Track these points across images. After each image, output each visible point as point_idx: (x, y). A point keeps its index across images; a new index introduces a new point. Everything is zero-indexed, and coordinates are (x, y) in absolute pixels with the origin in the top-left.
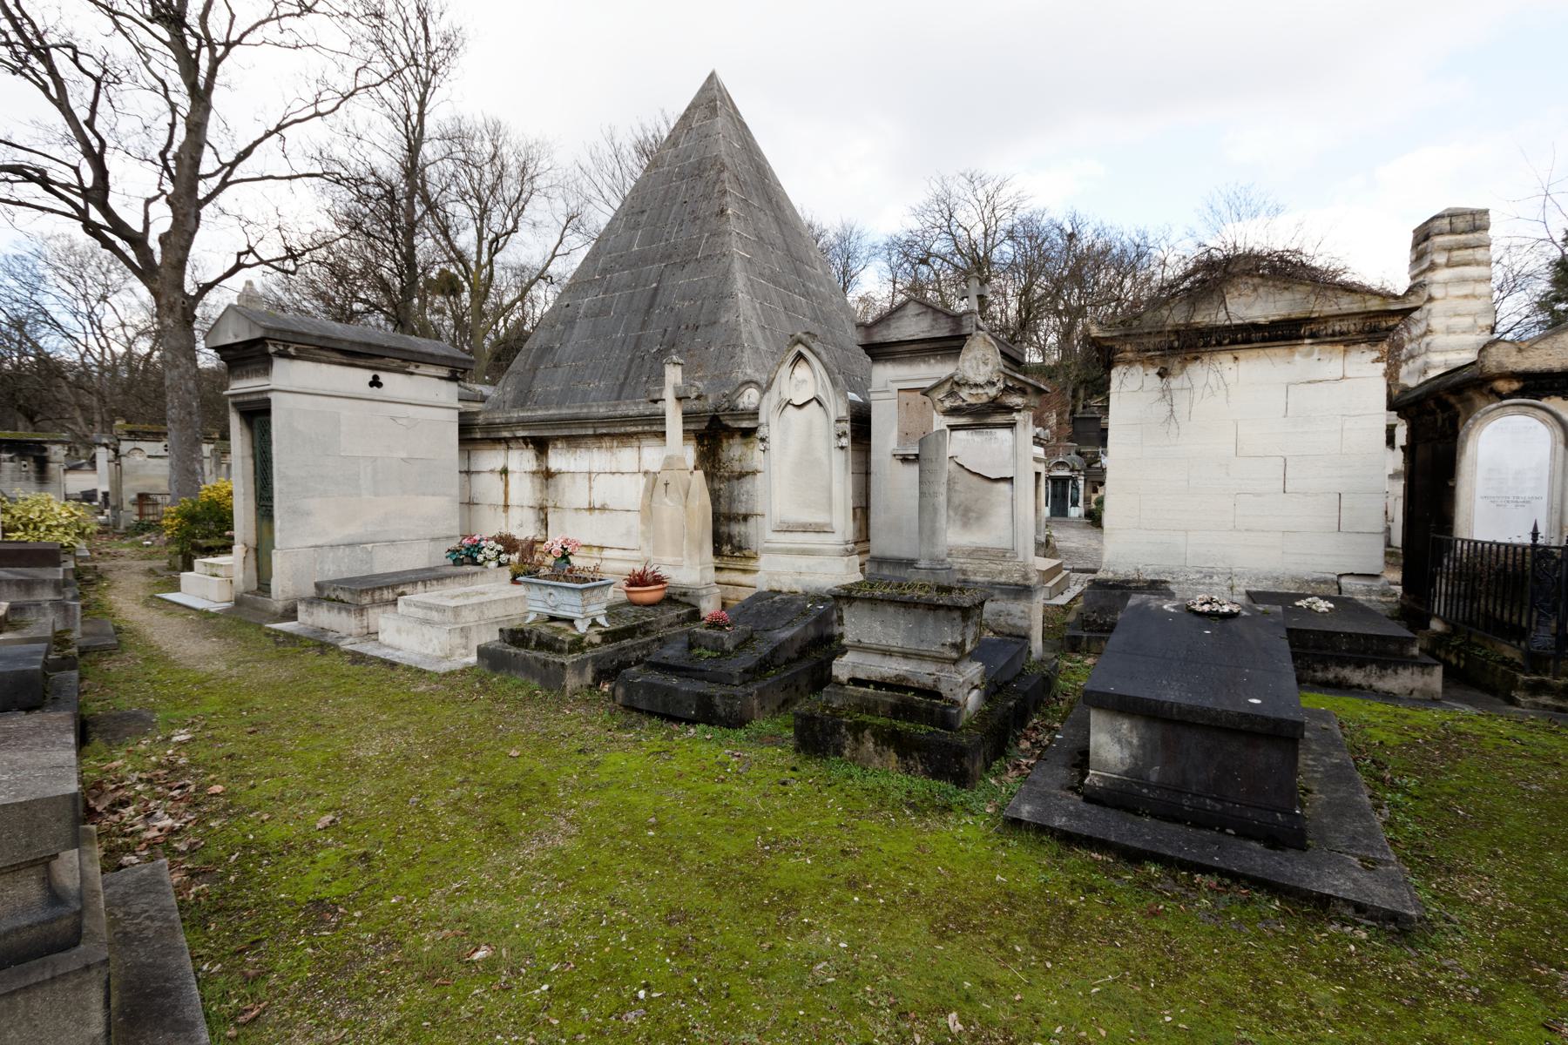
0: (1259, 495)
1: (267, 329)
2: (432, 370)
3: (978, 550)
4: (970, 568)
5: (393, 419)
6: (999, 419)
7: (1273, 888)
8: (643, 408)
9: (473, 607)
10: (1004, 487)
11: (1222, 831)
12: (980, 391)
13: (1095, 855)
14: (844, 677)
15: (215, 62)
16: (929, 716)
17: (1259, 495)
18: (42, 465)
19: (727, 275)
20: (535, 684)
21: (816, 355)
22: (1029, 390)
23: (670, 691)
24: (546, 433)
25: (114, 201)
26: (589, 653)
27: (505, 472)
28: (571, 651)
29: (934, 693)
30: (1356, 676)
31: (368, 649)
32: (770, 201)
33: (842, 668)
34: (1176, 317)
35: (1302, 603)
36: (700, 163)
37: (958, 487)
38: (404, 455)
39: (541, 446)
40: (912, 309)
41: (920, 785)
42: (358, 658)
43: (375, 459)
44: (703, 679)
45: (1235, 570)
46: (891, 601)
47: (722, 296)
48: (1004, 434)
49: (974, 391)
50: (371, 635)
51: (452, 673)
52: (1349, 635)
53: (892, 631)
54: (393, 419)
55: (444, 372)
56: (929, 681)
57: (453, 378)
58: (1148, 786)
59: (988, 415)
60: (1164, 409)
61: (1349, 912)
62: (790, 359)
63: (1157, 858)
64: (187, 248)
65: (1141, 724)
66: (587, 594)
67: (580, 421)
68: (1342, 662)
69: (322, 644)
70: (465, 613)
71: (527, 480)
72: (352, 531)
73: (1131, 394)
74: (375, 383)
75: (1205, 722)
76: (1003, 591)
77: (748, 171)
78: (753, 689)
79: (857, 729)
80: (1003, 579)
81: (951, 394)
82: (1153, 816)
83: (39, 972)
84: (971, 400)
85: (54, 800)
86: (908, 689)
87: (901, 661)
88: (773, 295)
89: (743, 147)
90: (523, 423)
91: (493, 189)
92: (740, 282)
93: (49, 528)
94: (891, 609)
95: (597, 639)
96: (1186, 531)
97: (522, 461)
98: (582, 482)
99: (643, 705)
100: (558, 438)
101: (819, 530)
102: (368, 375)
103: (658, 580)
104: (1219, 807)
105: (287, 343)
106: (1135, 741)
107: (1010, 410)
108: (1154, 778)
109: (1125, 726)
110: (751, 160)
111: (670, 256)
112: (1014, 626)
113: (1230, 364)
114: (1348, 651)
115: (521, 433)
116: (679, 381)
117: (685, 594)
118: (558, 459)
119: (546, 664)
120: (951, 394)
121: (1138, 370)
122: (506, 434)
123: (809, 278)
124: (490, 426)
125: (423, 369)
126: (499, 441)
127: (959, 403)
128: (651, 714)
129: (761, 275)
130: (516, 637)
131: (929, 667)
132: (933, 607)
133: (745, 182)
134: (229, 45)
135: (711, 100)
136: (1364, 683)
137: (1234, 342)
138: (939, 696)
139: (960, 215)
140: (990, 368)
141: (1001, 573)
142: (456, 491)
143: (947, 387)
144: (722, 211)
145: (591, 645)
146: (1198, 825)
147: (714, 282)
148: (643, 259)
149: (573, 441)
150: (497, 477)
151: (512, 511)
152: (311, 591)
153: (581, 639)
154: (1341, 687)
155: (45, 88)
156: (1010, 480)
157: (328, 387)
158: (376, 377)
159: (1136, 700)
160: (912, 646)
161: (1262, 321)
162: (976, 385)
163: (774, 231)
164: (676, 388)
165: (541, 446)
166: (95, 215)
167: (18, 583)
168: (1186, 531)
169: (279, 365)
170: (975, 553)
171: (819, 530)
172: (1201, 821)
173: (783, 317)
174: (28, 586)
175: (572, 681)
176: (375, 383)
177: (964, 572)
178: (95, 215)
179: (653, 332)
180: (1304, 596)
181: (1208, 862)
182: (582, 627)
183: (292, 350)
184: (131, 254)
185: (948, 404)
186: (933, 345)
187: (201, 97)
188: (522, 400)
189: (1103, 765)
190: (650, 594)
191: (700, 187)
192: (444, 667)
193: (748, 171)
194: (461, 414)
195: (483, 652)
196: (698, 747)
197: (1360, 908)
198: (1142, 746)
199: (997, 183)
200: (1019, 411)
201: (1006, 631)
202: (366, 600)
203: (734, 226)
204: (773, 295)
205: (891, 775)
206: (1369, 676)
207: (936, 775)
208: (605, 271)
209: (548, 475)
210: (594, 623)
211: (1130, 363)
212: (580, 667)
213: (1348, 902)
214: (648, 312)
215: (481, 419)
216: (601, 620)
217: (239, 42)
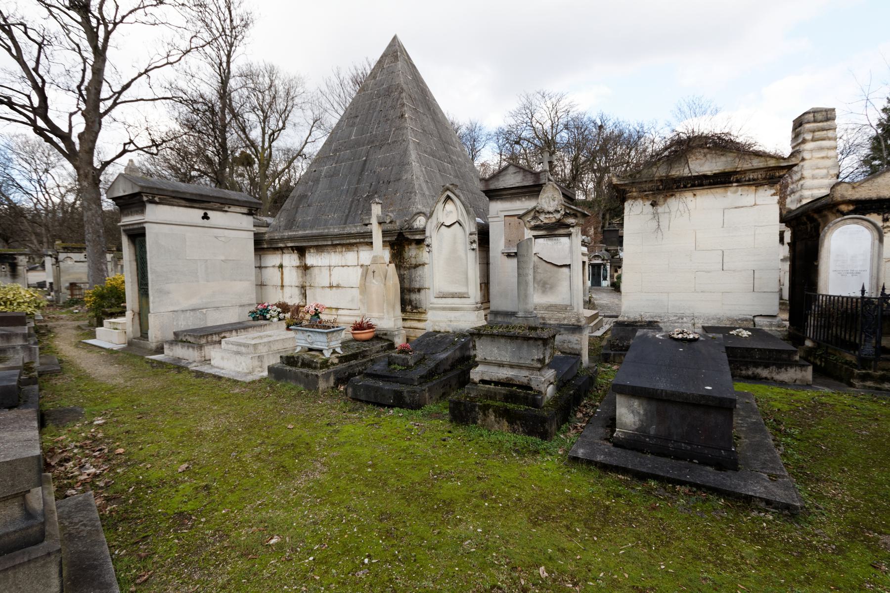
0: (709, 272)
1: (142, 187)
2: (238, 209)
3: (551, 306)
4: (547, 316)
5: (216, 237)
6: (562, 231)
8: (359, 229)
10: (565, 270)
11: (691, 461)
12: (551, 216)
14: (477, 379)
15: (108, 34)
16: (525, 400)
17: (709, 272)
19: (405, 152)
20: (301, 387)
21: (458, 197)
22: (579, 215)
23: (378, 389)
25: (51, 115)
26: (332, 369)
27: (281, 266)
28: (321, 368)
29: (528, 387)
30: (764, 373)
31: (205, 369)
33: (476, 374)
34: (660, 172)
35: (734, 332)
36: (389, 88)
38: (223, 258)
39: (301, 251)
41: (521, 439)
42: (199, 374)
45: (696, 314)
46: (503, 336)
47: (403, 164)
48: (565, 240)
50: (207, 361)
51: (254, 382)
53: (503, 353)
54: (216, 237)
55: (245, 210)
56: (525, 380)
57: (250, 214)
58: (649, 437)
59: (556, 229)
62: (443, 200)
63: (655, 477)
64: (94, 141)
66: (330, 336)
68: (757, 365)
69: (178, 367)
70: (260, 347)
72: (194, 302)
73: (636, 216)
74: (205, 217)
75: (681, 400)
76: (566, 329)
79: (485, 408)
80: (566, 322)
81: (535, 218)
82: (652, 454)
83: (20, 557)
86: (513, 385)
87: (509, 369)
88: (432, 163)
89: (413, 79)
90: (291, 239)
91: (270, 105)
92: (413, 156)
93: (19, 304)
94: (503, 341)
95: (336, 361)
97: (290, 260)
98: (325, 272)
99: (363, 398)
100: (311, 247)
101: (461, 296)
102: (201, 213)
103: (370, 327)
104: (689, 448)
105: (154, 195)
106: (642, 412)
107: (568, 226)
109: (636, 403)
110: (418, 86)
111: (373, 142)
112: (572, 348)
113: (693, 199)
114: (760, 358)
116: (380, 213)
117: (386, 334)
118: (311, 259)
119: (307, 376)
120: (535, 218)
121: (640, 202)
122: (281, 245)
124: (272, 241)
125: (233, 209)
126: (277, 249)
127: (539, 223)
128: (368, 402)
129: (425, 152)
130: (290, 360)
131: (525, 373)
132: (527, 339)
133: (415, 99)
134: (115, 24)
135: (395, 52)
136: (769, 376)
137: (693, 186)
138: (531, 389)
139: (537, 116)
140: (556, 202)
141: (564, 318)
142: (253, 278)
143: (532, 214)
145: (333, 364)
146: (677, 458)
148: (358, 144)
149: (320, 248)
150: (276, 270)
152: (171, 337)
153: (327, 361)
154: (756, 379)
155: (9, 50)
157: (178, 220)
158: (205, 214)
160: (515, 361)
161: (709, 173)
162: (549, 213)
163: (432, 126)
164: (378, 217)
165: (301, 251)
166: (40, 123)
170: (550, 308)
171: (461, 296)
173: (438, 176)
175: (322, 385)
176: (205, 217)
177: (544, 319)
178: (40, 123)
180: (735, 329)
182: (327, 354)
183: (157, 199)
184: (62, 145)
185: (533, 223)
186: (524, 190)
187: (100, 54)
188: (290, 225)
189: (624, 426)
190: (366, 335)
191: (389, 102)
192: (249, 378)
193: (416, 92)
194: (255, 234)
195: (271, 369)
196: (395, 420)
197: (768, 502)
198: (646, 414)
199: (558, 97)
201: (568, 351)
202: (203, 341)
203: (409, 124)
205: (505, 435)
206: (771, 372)
207: (530, 433)
208: (336, 151)
209: (306, 268)
210: (334, 352)
211: (635, 198)
212: (326, 377)
215: (267, 237)
217: (121, 22)
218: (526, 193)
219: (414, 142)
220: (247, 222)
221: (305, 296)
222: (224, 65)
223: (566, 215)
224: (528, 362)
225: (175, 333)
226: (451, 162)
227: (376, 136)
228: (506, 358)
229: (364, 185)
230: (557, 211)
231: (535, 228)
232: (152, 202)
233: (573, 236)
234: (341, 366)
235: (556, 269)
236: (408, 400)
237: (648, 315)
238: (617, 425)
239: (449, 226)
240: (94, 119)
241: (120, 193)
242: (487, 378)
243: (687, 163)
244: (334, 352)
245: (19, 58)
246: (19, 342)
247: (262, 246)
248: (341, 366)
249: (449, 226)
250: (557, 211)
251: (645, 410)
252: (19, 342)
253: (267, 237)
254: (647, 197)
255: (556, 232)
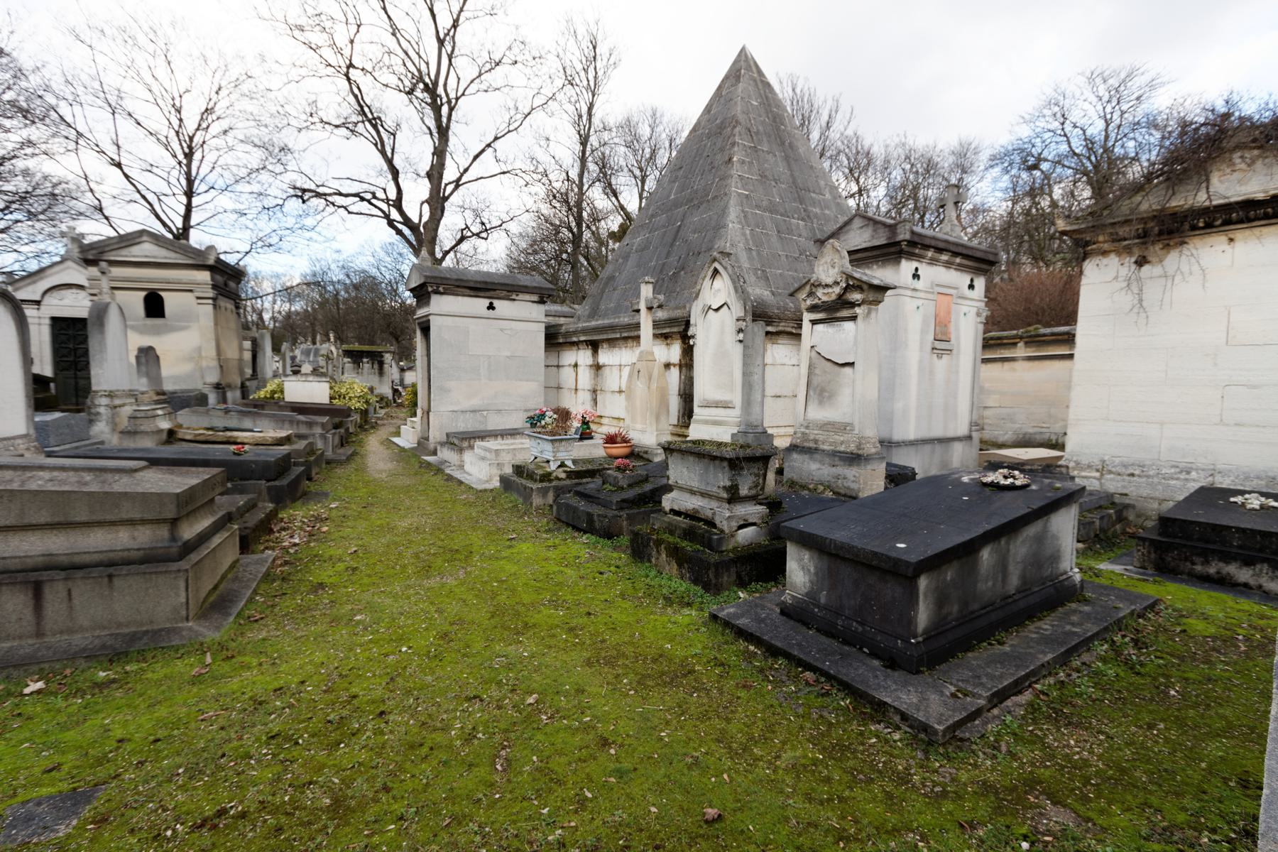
0: (1255, 387)
2: (527, 297)
3: (829, 423)
4: (821, 438)
6: (845, 313)
7: (847, 688)
8: (625, 320)
9: (508, 451)
10: (848, 370)
11: (861, 649)
12: (830, 290)
13: (752, 648)
15: (451, 109)
16: (709, 545)
17: (1255, 387)
18: (381, 364)
19: (724, 212)
21: (725, 268)
22: (865, 287)
23: (575, 510)
24: (595, 338)
26: (554, 483)
27: (576, 365)
28: (541, 481)
29: (711, 524)
30: (1243, 575)
31: (458, 474)
32: (783, 143)
33: (668, 501)
34: (1148, 203)
35: (1239, 499)
36: (722, 122)
37: (817, 371)
38: (508, 354)
39: (595, 346)
40: (858, 222)
41: (683, 586)
43: (489, 357)
44: (598, 504)
45: (1219, 467)
46: (692, 453)
48: (849, 325)
49: (826, 291)
50: (461, 467)
51: (485, 490)
52: (1244, 531)
55: (535, 298)
56: (709, 514)
57: (542, 302)
58: (818, 607)
59: (838, 310)
60: (1127, 300)
61: (897, 718)
62: (710, 273)
63: (788, 656)
64: (436, 230)
65: (816, 556)
66: (557, 444)
67: (612, 328)
68: (1227, 558)
69: (438, 470)
70: (503, 454)
71: (587, 370)
72: (475, 402)
73: (1102, 284)
74: (491, 307)
76: (841, 459)
77: (763, 123)
78: (624, 514)
80: (842, 448)
81: (811, 294)
82: (818, 630)
83: (162, 567)
84: (825, 299)
85: (168, 495)
86: (700, 520)
90: (584, 331)
91: (648, 161)
92: (733, 213)
93: (350, 398)
94: (691, 458)
95: (563, 476)
96: (1162, 424)
97: (583, 357)
98: (616, 371)
99: (563, 518)
101: (726, 406)
102: (486, 302)
103: (625, 440)
104: (860, 629)
105: (438, 285)
106: (812, 569)
107: (852, 305)
108: (823, 601)
109: (806, 555)
110: (768, 111)
112: (848, 488)
113: (1226, 247)
114: (1240, 547)
115: (582, 338)
116: (650, 295)
117: (646, 452)
118: (605, 356)
119: (525, 488)
120: (811, 294)
121: (1112, 261)
122: (575, 339)
123: (814, 203)
124: (568, 334)
125: (521, 296)
126: (573, 344)
127: (816, 301)
128: (568, 525)
129: (758, 207)
130: (519, 470)
131: (714, 504)
132: (714, 458)
133: (757, 133)
134: (457, 99)
135: (744, 70)
136: (1252, 582)
137: (1228, 222)
138: (714, 526)
139: (1075, 116)
140: (836, 270)
141: (842, 443)
142: (542, 378)
143: (808, 288)
144: (730, 159)
145: (558, 479)
146: (845, 642)
147: (715, 217)
148: (676, 204)
149: (612, 342)
150: (571, 370)
151: (580, 393)
152: (444, 439)
153: (550, 474)
154: (1223, 583)
155: (376, 145)
156: (851, 364)
157: (463, 311)
158: (491, 304)
159: (811, 535)
160: (703, 487)
161: (1260, 196)
162: (827, 286)
163: (782, 168)
164: (647, 300)
165: (595, 346)
166: (395, 215)
167: (306, 423)
168: (1162, 424)
169: (435, 299)
171: (726, 406)
172: (848, 639)
173: (774, 239)
174: (310, 425)
175: (537, 500)
176: (491, 307)
177: (816, 441)
178: (395, 215)
179: (673, 259)
181: (820, 666)
182: (553, 466)
183: (441, 289)
185: (809, 302)
186: (875, 253)
187: (443, 132)
188: (593, 314)
189: (794, 588)
190: (618, 450)
192: (480, 487)
193: (763, 123)
194: (547, 328)
195: (503, 479)
196: (580, 546)
197: (904, 717)
198: (816, 574)
199: (1123, 76)
200: (859, 305)
201: (842, 491)
202: (465, 444)
203: (736, 170)
204: (769, 223)
205: (673, 580)
206: (1259, 575)
207: (695, 581)
209: (598, 367)
210: (562, 465)
211: (1105, 253)
212: (544, 492)
213: (897, 711)
214: (672, 245)
215: (563, 329)
216: (569, 463)
218: (878, 256)
219: (739, 194)
220: (538, 312)
221: (595, 401)
222: (585, 118)
223: (846, 289)
224: (715, 489)
225: (448, 435)
226: (807, 217)
227: (696, 192)
228: (695, 484)
229: (673, 259)
230: (837, 283)
231: (813, 309)
232: (437, 292)
233: (859, 319)
234: (568, 482)
235: (837, 368)
236: (597, 525)
237: (1117, 460)
238: (788, 585)
239: (717, 310)
240: (437, 202)
241: (413, 285)
242: (676, 508)
243: (1208, 180)
244: (562, 465)
245: (383, 152)
246: (318, 430)
247: (555, 340)
248: (568, 482)
249: (717, 310)
250: (837, 283)
251: (816, 567)
252: (318, 430)
253: (563, 329)
254: (1128, 250)
255: (838, 315)
